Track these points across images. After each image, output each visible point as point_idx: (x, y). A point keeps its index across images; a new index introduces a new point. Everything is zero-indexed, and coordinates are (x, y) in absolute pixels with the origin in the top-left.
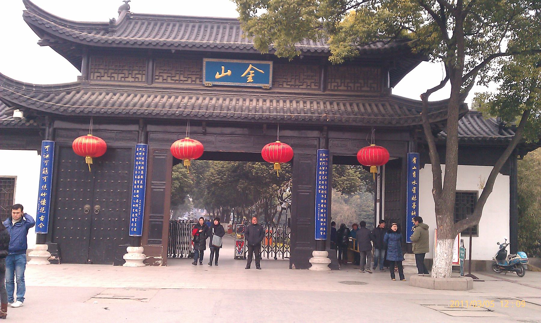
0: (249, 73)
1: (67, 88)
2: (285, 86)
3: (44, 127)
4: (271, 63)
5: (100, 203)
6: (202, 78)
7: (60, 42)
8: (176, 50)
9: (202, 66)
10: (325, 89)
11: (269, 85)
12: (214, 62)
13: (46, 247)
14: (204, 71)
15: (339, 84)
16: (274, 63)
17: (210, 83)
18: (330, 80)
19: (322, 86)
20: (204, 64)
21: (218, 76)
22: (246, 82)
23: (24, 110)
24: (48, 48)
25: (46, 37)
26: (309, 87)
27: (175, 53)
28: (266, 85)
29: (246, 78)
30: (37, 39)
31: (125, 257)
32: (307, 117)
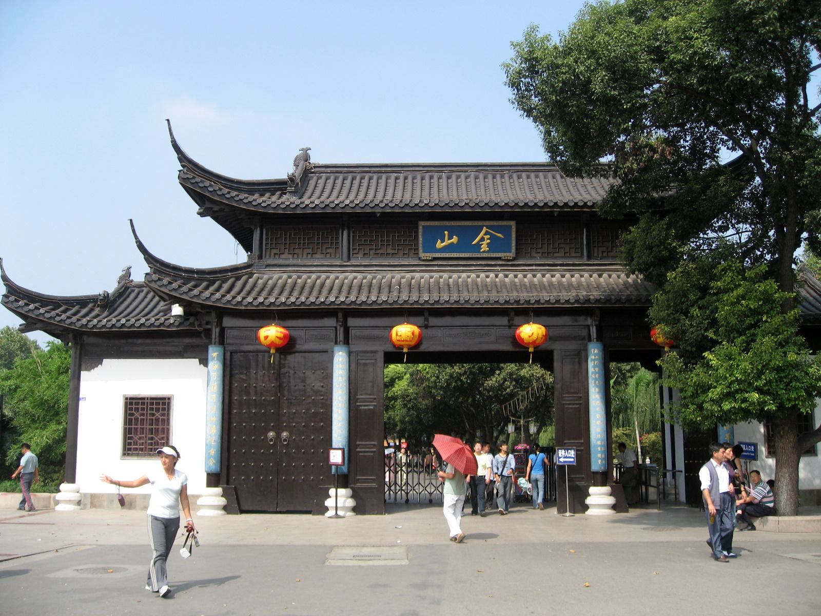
0: (483, 240)
1: (235, 271)
2: (534, 254)
3: (209, 327)
4: (513, 224)
5: (289, 428)
6: (418, 249)
7: (227, 210)
8: (382, 213)
9: (417, 232)
10: (589, 258)
11: (511, 255)
12: (468, 226)
13: (219, 490)
14: (421, 239)
15: (610, 249)
16: (517, 224)
17: (430, 255)
18: (596, 244)
19: (585, 254)
20: (420, 228)
21: (439, 245)
22: (479, 252)
23: (184, 304)
24: (208, 219)
25: (208, 205)
26: (567, 255)
27: (380, 216)
28: (508, 254)
29: (478, 245)
30: (196, 208)
31: (588, 501)
32: (592, 297)
